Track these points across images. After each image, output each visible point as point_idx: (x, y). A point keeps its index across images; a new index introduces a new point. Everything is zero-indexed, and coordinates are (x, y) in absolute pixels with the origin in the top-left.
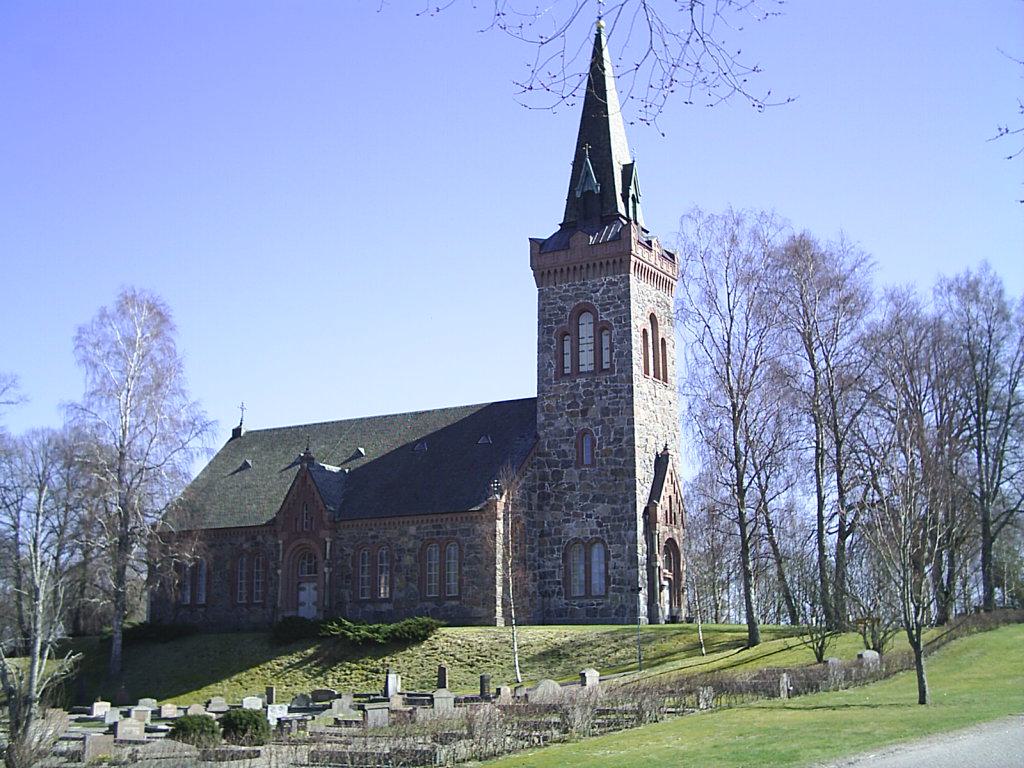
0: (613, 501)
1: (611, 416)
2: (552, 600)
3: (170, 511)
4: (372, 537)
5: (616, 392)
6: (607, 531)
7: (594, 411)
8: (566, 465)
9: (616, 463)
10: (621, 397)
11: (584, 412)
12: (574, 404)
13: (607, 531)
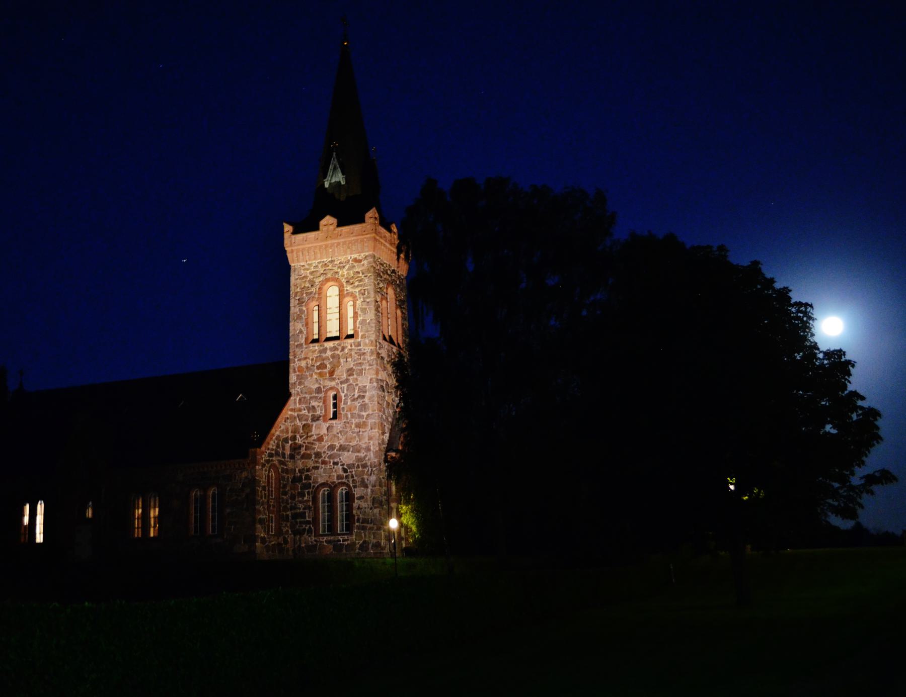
7: (341, 373)
8: (315, 419)
11: (332, 373)
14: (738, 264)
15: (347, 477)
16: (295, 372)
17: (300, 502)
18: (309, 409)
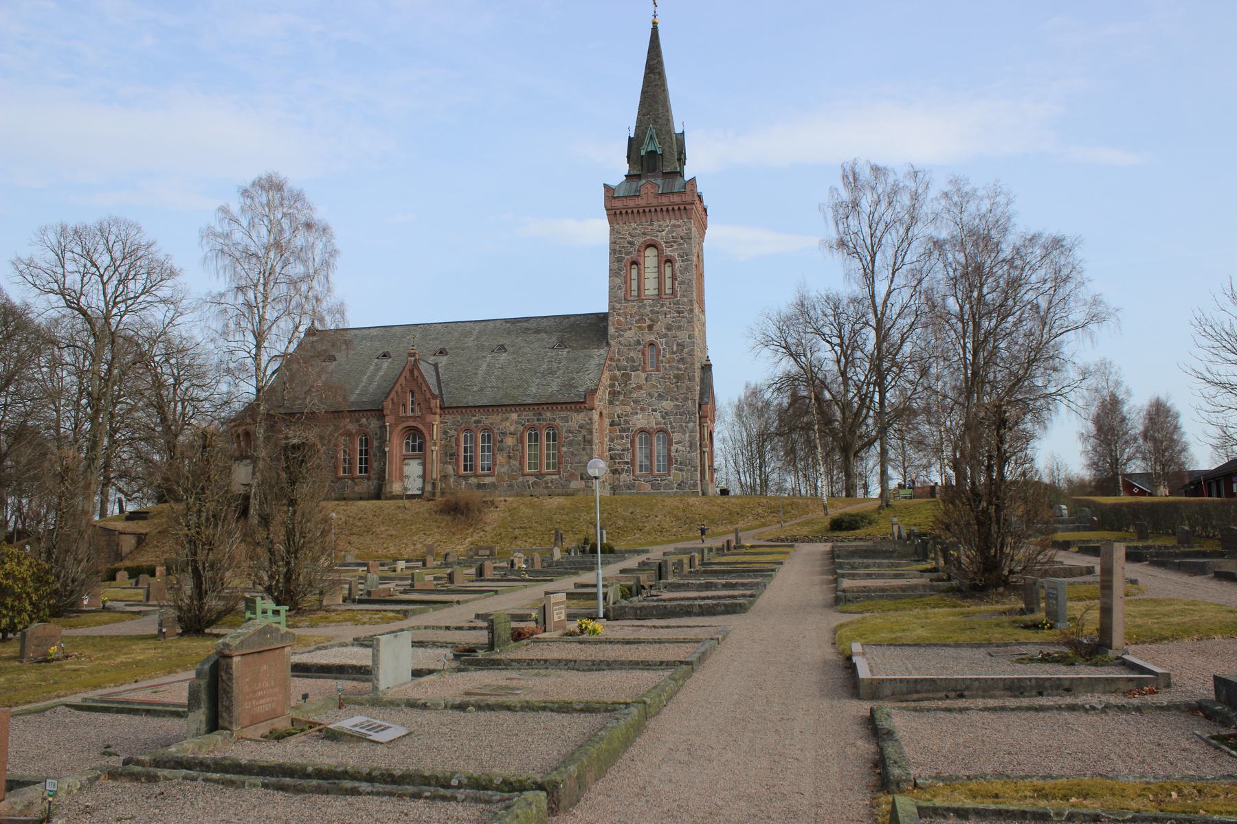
0: (674, 399)
1: (674, 332)
2: (622, 476)
3: (1093, 426)
4: (475, 422)
5: (679, 312)
6: (671, 423)
7: (660, 327)
8: (635, 369)
9: (678, 369)
10: (683, 317)
11: (650, 327)
12: (642, 320)
13: (671, 423)
14: (789, 372)
15: (665, 423)
16: (613, 325)
17: (619, 445)
18: (628, 359)
